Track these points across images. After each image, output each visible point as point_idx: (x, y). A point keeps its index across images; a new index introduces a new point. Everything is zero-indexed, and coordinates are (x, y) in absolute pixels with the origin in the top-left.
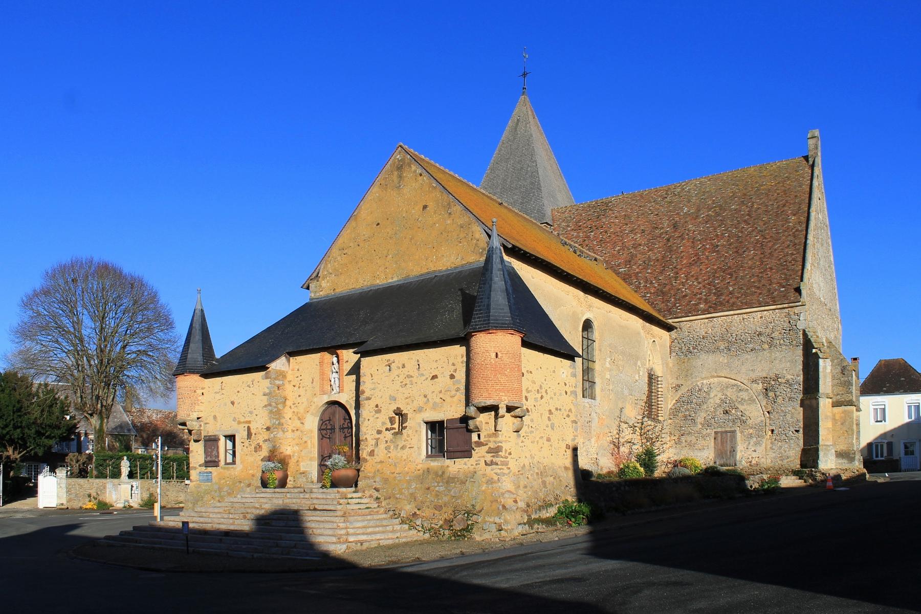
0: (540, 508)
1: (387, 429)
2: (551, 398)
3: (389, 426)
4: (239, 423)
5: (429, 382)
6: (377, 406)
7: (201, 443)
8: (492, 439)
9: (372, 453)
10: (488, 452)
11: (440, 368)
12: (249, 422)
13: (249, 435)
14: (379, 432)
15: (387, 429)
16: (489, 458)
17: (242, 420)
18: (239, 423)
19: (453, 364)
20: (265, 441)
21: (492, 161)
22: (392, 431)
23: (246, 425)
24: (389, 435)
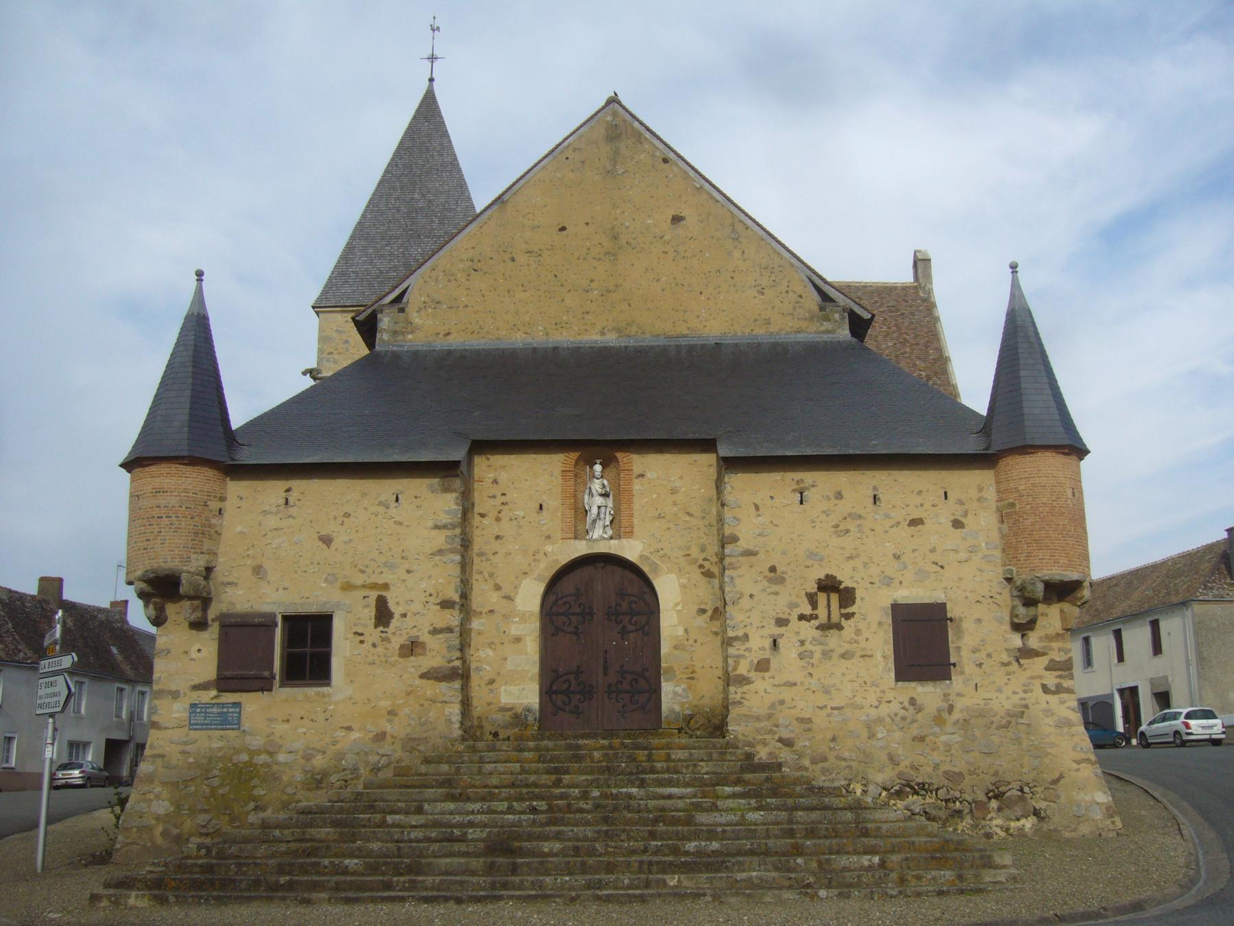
0: (763, 885)
1: (802, 617)
2: (989, 656)
3: (807, 610)
4: (348, 587)
5: (904, 532)
6: (773, 569)
7: (214, 630)
8: (1055, 645)
9: (762, 666)
10: (1047, 669)
11: (927, 506)
12: (386, 586)
13: (383, 615)
14: (782, 622)
15: (802, 617)
16: (1051, 679)
17: (359, 580)
18: (348, 587)
19: (961, 503)
20: (435, 632)
21: (119, 658)
22: (815, 623)
23: (374, 595)
24: (808, 630)
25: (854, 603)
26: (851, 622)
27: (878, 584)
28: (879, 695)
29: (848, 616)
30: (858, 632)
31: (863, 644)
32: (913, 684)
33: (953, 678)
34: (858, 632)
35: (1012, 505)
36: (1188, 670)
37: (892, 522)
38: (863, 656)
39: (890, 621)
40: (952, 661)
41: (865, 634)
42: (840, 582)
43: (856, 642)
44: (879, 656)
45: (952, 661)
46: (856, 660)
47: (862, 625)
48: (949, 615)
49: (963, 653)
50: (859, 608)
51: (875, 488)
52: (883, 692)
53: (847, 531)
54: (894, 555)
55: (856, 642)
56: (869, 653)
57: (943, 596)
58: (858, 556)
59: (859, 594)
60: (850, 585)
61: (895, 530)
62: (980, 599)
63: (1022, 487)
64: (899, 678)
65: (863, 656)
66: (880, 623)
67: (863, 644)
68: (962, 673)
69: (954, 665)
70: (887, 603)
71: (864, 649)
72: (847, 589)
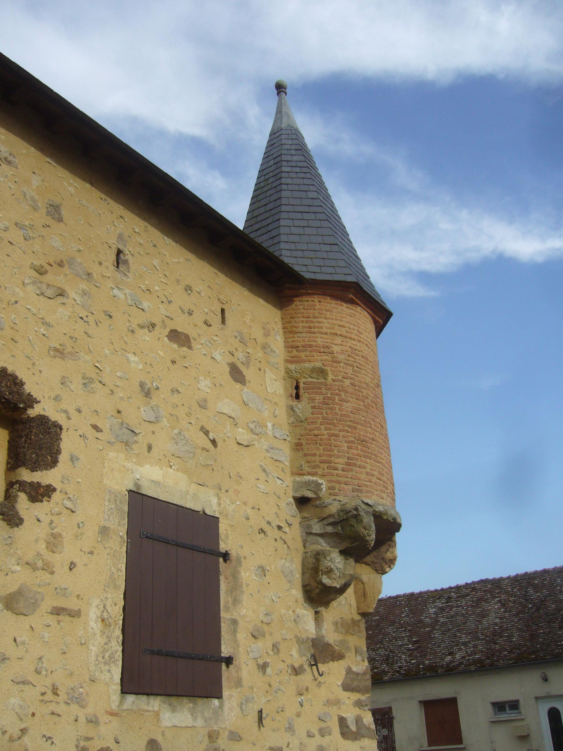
25: (54, 463)
26: (41, 509)
27: (105, 436)
28: (84, 729)
29: (39, 493)
30: (54, 542)
31: (62, 578)
32: (155, 704)
33: (226, 693)
34: (54, 542)
35: (322, 372)
36: (313, 673)
37: (143, 319)
38: (58, 611)
39: (123, 531)
40: (225, 651)
41: (70, 551)
42: (31, 401)
43: (48, 568)
44: (93, 614)
45: (225, 651)
46: (41, 618)
47: (65, 525)
48: (223, 547)
49: (242, 636)
50: (64, 479)
51: (120, 237)
52: (93, 721)
53: (61, 294)
54: (175, 362)
55: (48, 568)
56: (72, 604)
57: (215, 507)
58: (74, 355)
59: (68, 444)
60: (54, 416)
61: (145, 336)
62: (266, 528)
63: (336, 349)
64: (132, 683)
65: (58, 611)
66: (104, 531)
67: (62, 578)
68: (239, 683)
69: (229, 661)
70: (121, 484)
71: (63, 592)
72: (43, 420)
